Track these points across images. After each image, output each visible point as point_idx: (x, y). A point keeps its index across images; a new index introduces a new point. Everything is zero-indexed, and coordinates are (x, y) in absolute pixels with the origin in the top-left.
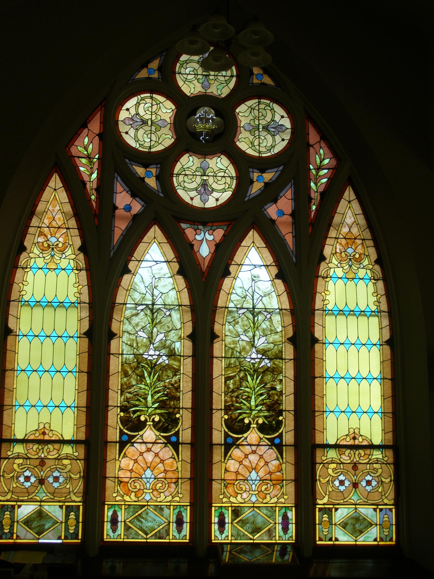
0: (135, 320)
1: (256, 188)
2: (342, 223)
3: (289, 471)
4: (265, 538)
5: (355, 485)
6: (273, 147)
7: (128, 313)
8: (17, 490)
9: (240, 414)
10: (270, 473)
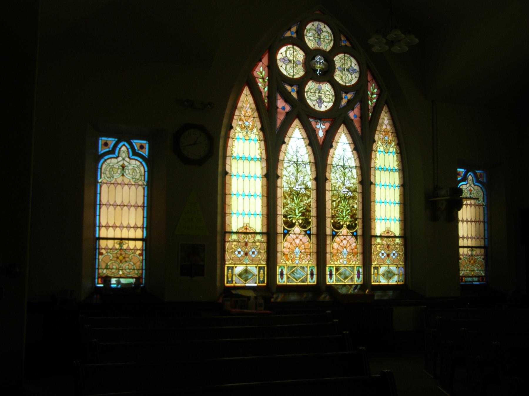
0: (289, 169)
1: (344, 102)
2: (382, 124)
3: (359, 249)
4: (350, 281)
5: (388, 255)
6: (351, 80)
7: (285, 165)
8: (235, 258)
9: (339, 220)
10: (352, 250)
